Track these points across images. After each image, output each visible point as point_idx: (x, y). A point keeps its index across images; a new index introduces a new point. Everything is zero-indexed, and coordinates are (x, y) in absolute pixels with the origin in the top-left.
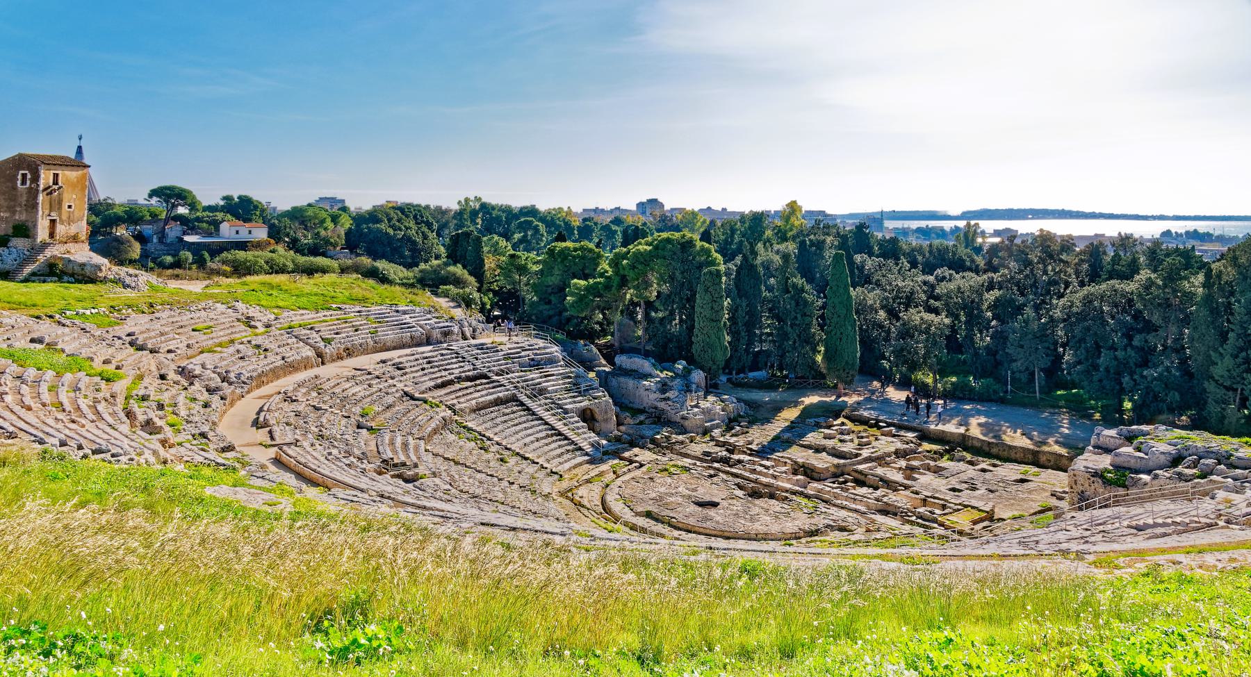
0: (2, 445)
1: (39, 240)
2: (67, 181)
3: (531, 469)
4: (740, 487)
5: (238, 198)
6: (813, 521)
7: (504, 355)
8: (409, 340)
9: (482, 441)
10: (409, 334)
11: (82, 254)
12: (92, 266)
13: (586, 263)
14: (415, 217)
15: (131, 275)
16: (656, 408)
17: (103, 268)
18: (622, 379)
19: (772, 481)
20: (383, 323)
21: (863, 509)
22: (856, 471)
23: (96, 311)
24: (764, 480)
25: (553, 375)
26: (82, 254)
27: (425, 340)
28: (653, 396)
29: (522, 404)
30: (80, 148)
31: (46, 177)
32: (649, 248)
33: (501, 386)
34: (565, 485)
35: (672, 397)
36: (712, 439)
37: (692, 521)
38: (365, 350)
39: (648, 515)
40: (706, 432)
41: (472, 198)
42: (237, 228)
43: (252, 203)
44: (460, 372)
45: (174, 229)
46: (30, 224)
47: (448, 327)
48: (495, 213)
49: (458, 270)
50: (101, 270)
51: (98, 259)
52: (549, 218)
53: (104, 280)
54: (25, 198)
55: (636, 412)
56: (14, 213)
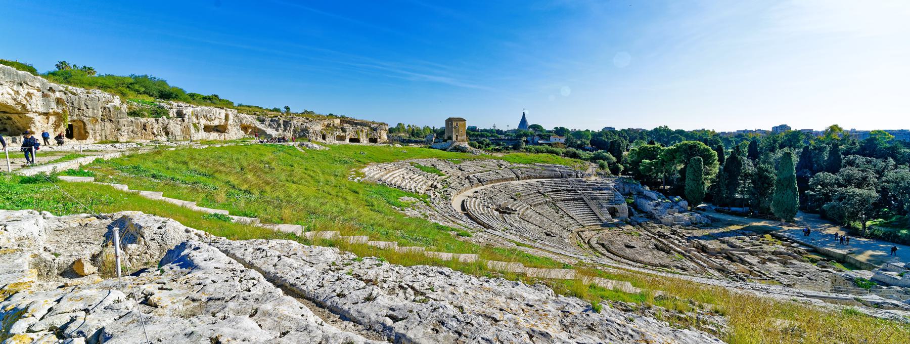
8: (554, 176)
16: (651, 212)
18: (641, 200)
26: (465, 145)
28: (651, 208)
29: (585, 201)
31: (454, 124)
53: (468, 152)
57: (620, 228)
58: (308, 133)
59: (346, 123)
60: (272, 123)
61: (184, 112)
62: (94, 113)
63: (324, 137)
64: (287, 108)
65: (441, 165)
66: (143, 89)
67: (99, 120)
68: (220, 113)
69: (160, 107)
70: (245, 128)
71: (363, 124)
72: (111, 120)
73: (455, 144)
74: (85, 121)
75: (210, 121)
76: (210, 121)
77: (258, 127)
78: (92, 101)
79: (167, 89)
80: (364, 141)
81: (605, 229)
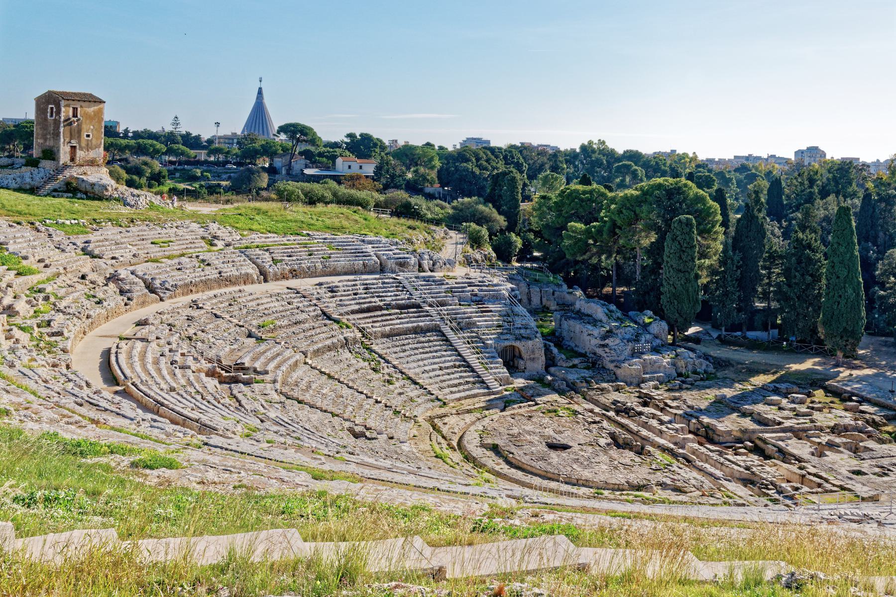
1: (61, 163)
2: (86, 115)
5: (360, 136)
7: (448, 288)
9: (377, 362)
10: (361, 262)
11: (100, 176)
12: (100, 186)
14: (505, 158)
15: (134, 196)
16: (595, 354)
17: (110, 189)
20: (341, 250)
21: (718, 473)
23: (76, 221)
25: (491, 311)
26: (100, 176)
27: (379, 269)
28: (594, 342)
30: (260, 89)
31: (66, 112)
32: (638, 193)
33: (427, 316)
35: (611, 344)
38: (311, 273)
39: (495, 449)
41: (596, 141)
42: (350, 163)
43: (372, 141)
44: (393, 300)
45: (299, 162)
46: (55, 149)
47: (404, 258)
50: (107, 190)
53: (109, 199)
54: (52, 128)
56: (45, 140)
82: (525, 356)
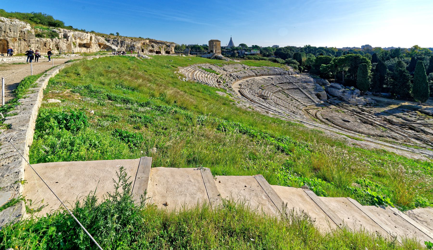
0: (3, 67)
3: (299, 103)
4: (360, 119)
6: (382, 133)
9: (288, 96)
11: (220, 55)
13: (327, 61)
14: (290, 49)
18: (331, 88)
19: (374, 121)
21: (406, 135)
22: (411, 126)
24: (370, 120)
26: (220, 55)
29: (300, 90)
31: (214, 43)
34: (307, 108)
36: (358, 107)
37: (339, 123)
38: (266, 75)
39: (327, 119)
40: (357, 105)
48: (311, 49)
49: (295, 61)
51: (222, 56)
52: (327, 50)
53: (223, 59)
55: (334, 96)
57: (328, 107)
58: (135, 48)
59: (152, 42)
60: (114, 42)
61: (68, 35)
62: (14, 35)
63: (143, 51)
64: (118, 33)
65: (214, 68)
66: (39, 21)
67: (18, 39)
68: (87, 36)
69: (53, 32)
70: (100, 45)
71: (162, 43)
72: (25, 40)
73: (215, 55)
74: (8, 40)
75: (82, 41)
76: (82, 41)
77: (107, 44)
78: (14, 26)
79: (53, 21)
80: (163, 53)
81: (320, 108)
82: (321, 95)
